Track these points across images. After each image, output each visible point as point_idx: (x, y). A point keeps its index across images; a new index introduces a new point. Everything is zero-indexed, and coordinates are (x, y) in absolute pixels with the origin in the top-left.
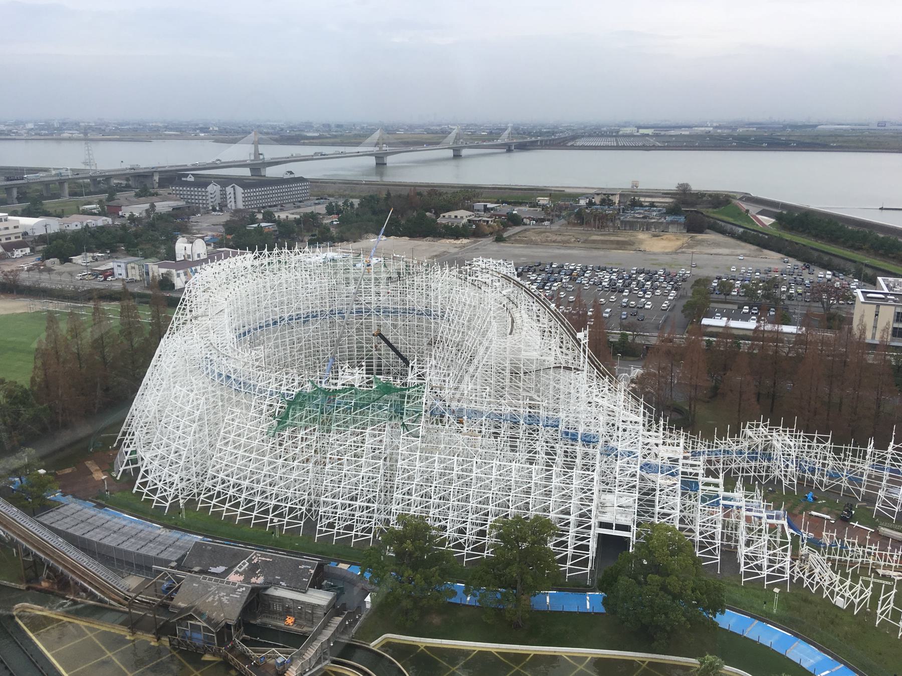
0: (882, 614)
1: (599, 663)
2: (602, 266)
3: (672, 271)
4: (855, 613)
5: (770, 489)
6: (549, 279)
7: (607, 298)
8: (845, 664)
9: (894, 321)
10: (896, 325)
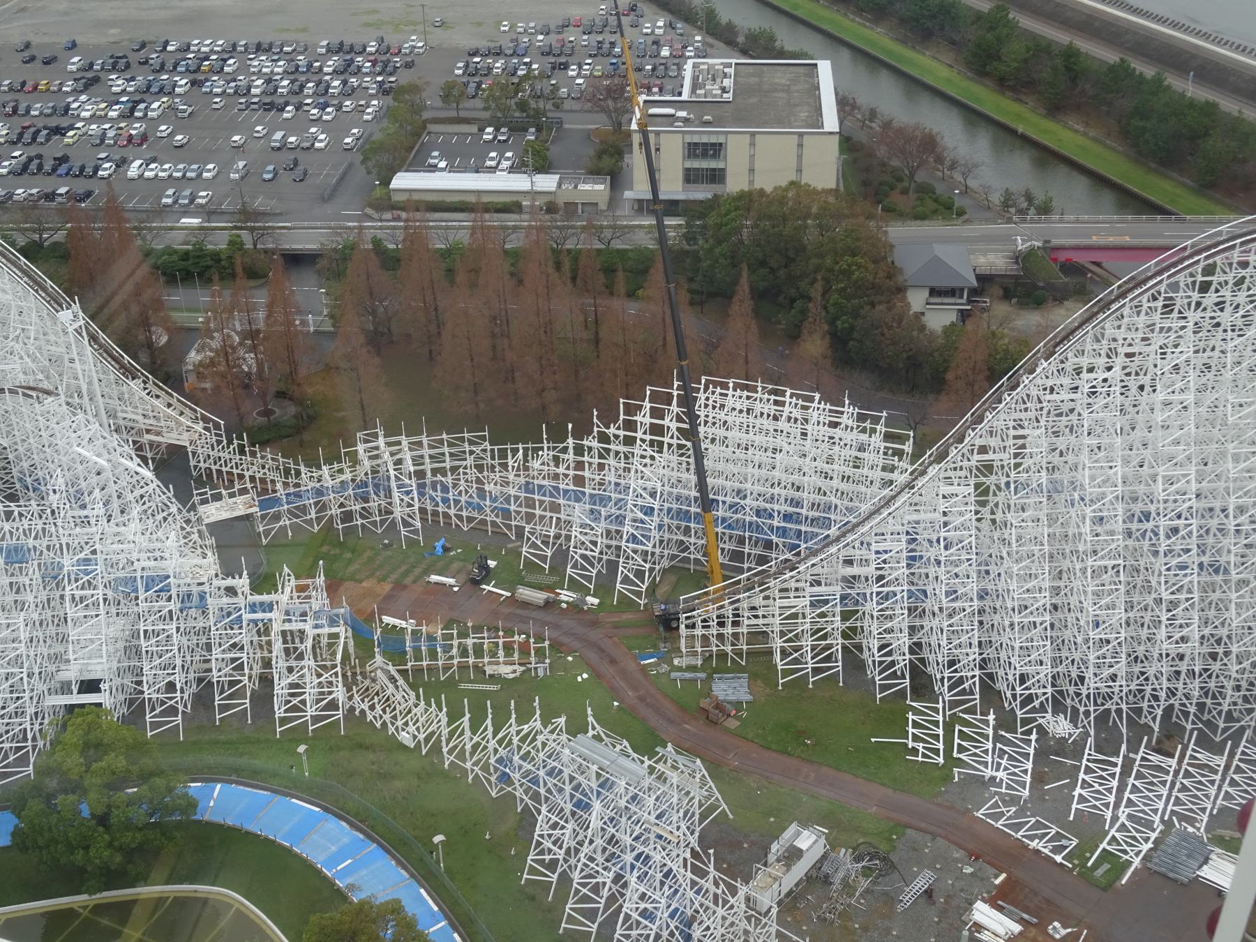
0: (450, 752)
1: (58, 919)
2: (266, 40)
3: (392, 39)
4: (424, 753)
5: (386, 541)
6: (149, 87)
7: (248, 130)
8: (380, 844)
9: (684, 157)
10: (688, 164)
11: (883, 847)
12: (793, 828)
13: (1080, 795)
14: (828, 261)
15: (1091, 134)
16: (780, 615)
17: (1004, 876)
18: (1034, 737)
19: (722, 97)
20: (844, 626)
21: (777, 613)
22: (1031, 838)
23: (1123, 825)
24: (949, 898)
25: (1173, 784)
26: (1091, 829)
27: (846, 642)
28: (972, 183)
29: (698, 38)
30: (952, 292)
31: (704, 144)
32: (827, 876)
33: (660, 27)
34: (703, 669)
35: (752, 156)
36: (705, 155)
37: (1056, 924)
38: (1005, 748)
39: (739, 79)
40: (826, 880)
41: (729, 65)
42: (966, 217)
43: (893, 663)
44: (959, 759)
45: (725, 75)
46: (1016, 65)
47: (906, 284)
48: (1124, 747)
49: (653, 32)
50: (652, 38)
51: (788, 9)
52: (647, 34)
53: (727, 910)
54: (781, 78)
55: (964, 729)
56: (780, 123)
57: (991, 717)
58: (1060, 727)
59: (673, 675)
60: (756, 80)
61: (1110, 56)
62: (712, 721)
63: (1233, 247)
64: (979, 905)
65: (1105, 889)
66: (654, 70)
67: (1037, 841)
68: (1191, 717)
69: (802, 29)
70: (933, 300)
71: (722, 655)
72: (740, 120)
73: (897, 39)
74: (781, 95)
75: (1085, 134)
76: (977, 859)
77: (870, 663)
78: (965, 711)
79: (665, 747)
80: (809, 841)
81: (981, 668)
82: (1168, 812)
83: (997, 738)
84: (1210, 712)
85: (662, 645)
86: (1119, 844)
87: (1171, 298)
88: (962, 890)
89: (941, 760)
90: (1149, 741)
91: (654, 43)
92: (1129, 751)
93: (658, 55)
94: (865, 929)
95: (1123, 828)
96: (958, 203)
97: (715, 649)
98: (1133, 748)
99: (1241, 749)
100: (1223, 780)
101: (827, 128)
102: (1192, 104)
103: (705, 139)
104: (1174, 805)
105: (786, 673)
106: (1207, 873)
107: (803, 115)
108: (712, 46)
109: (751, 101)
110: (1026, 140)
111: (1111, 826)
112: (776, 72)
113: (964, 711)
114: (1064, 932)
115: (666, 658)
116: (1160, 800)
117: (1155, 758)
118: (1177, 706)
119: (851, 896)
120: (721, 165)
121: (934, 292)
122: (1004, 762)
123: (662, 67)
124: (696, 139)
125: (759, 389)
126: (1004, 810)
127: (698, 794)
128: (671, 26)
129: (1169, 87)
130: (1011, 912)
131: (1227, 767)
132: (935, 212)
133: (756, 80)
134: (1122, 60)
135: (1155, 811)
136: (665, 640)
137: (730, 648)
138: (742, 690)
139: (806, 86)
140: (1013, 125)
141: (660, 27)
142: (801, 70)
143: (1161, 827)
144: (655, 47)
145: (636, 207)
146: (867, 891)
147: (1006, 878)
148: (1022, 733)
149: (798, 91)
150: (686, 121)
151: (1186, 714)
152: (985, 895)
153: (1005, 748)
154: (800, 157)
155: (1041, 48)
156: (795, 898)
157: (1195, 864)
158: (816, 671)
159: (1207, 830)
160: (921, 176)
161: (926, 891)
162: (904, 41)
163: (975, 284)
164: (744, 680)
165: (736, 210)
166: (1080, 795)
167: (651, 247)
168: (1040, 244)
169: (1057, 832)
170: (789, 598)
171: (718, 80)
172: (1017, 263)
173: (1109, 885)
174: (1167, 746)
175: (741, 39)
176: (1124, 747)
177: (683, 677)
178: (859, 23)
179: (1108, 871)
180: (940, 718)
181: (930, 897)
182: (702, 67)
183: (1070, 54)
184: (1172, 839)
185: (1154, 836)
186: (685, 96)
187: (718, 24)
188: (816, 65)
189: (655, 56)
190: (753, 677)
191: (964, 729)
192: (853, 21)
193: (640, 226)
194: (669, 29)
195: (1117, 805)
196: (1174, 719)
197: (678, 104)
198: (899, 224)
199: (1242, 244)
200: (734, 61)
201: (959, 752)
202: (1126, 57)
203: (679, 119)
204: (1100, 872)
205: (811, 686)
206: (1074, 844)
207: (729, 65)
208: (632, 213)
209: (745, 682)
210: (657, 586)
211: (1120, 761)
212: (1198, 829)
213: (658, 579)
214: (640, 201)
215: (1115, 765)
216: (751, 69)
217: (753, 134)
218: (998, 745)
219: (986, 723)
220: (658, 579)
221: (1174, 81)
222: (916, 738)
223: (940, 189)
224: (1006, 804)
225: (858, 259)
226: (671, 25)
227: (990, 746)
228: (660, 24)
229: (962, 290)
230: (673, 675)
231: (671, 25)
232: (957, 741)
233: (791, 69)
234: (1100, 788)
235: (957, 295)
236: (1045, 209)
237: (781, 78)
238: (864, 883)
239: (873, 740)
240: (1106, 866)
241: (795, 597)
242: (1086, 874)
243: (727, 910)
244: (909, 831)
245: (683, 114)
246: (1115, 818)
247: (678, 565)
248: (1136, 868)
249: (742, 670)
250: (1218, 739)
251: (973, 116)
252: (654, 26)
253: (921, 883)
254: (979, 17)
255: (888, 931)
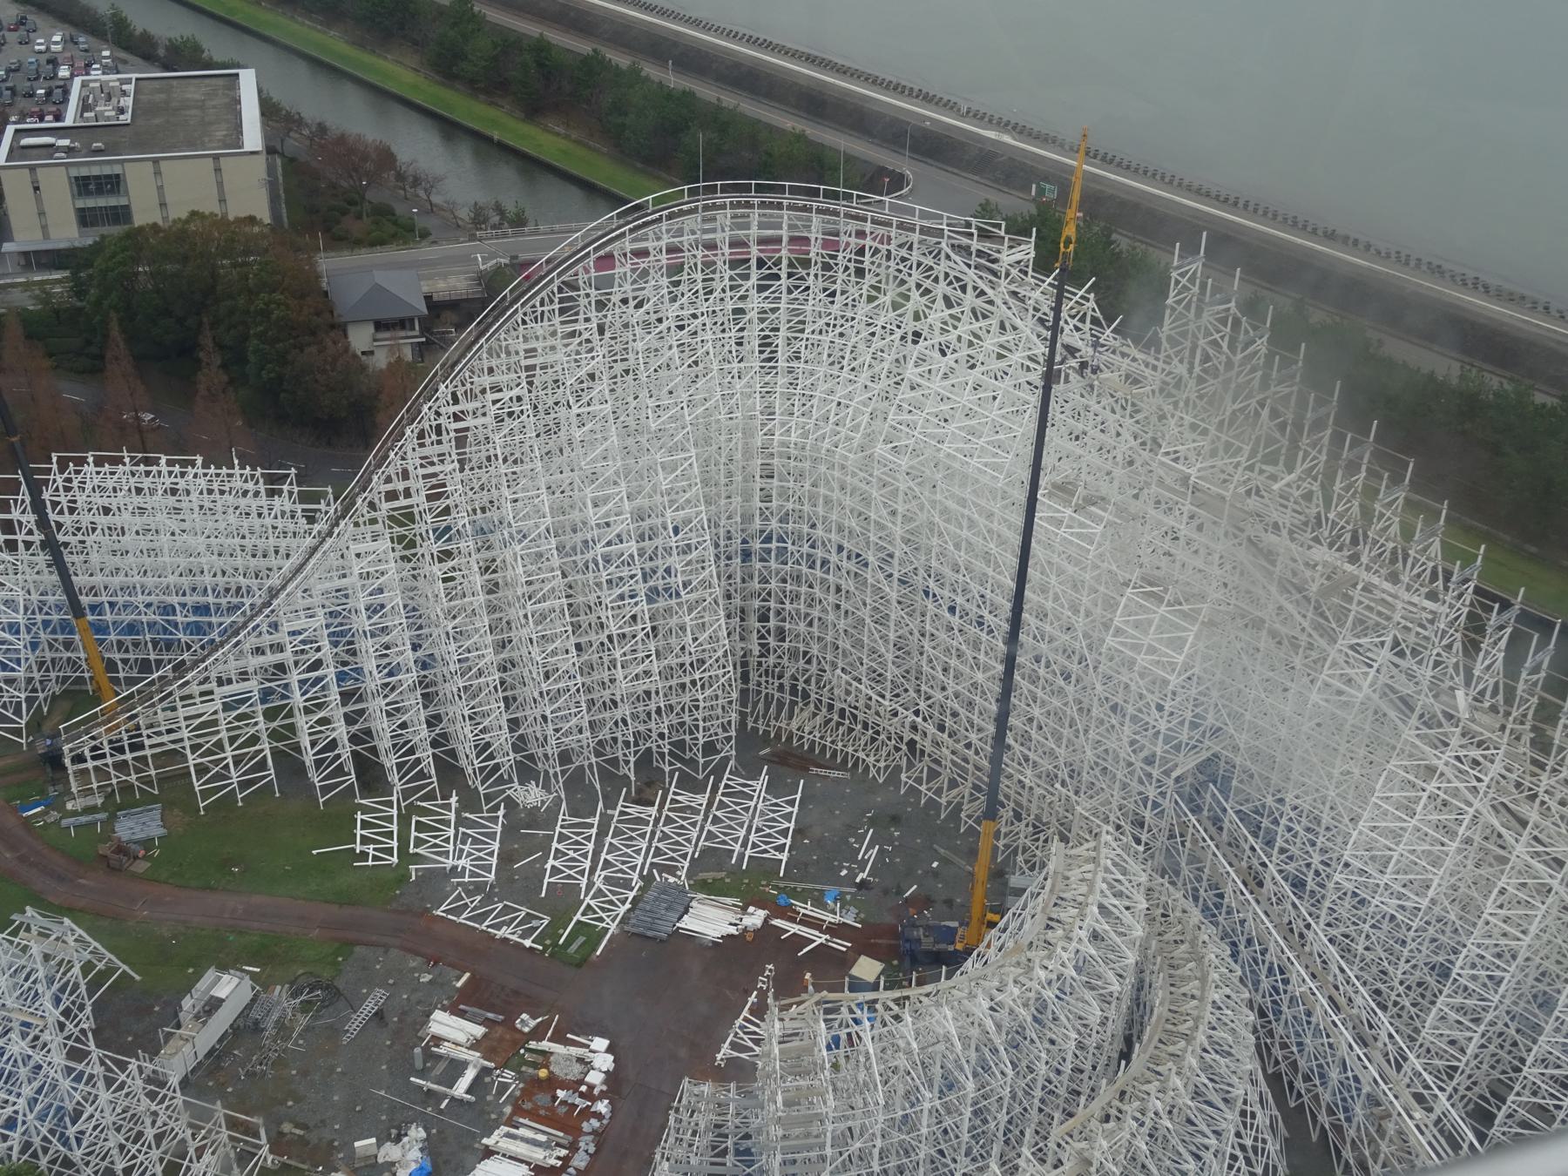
9: (73, 196)
10: (81, 204)
11: (326, 974)
12: (211, 974)
13: (553, 867)
14: (241, 301)
15: (573, 136)
16: (187, 727)
17: (467, 975)
18: (501, 813)
19: (118, 119)
20: (433, 734)
21: (183, 724)
22: (498, 927)
23: (600, 890)
24: (403, 1014)
25: (653, 833)
26: (564, 900)
27: (358, 748)
28: (435, 199)
29: (106, 53)
30: (403, 324)
31: (97, 177)
32: (256, 1023)
33: (56, 43)
34: (104, 808)
35: (160, 188)
36: (100, 191)
37: (524, 1016)
38: (468, 831)
39: (142, 97)
40: (257, 1028)
41: (128, 81)
42: (431, 238)
43: (497, 767)
44: (417, 854)
45: (124, 93)
46: (484, 63)
47: (343, 320)
48: (601, 805)
49: (48, 49)
50: (46, 56)
51: (223, 14)
52: (40, 52)
53: (114, 1092)
54: (194, 93)
55: (421, 819)
56: (193, 146)
57: (454, 800)
58: (531, 796)
59: (64, 822)
60: (163, 96)
61: (584, 47)
62: (113, 869)
63: (623, 234)
64: (438, 1015)
65: (579, 966)
66: (49, 94)
67: (505, 928)
68: (667, 757)
69: (246, 37)
70: (380, 335)
71: (126, 788)
72: (140, 144)
73: (354, 43)
74: (193, 112)
75: (567, 137)
76: (436, 963)
77: (471, 771)
78: (424, 798)
79: (24, 912)
80: (229, 987)
81: (598, 754)
82: (647, 866)
83: (461, 822)
84: (691, 750)
85: (51, 789)
86: (595, 912)
87: (571, 299)
88: (419, 1003)
89: (395, 860)
90: (628, 792)
91: (49, 62)
92: (606, 807)
93: (55, 76)
94: (304, 1073)
95: (600, 893)
96: (421, 223)
97: (114, 781)
98: (610, 803)
99: (724, 781)
100: (705, 820)
101: (248, 147)
102: (669, 95)
103: (95, 171)
104: (653, 857)
105: (206, 794)
106: (688, 923)
107: (220, 134)
108: (125, 62)
109: (157, 121)
110: (503, 147)
111: (586, 896)
112: (189, 85)
113: (422, 799)
114: (533, 1023)
115: (56, 804)
116: (639, 854)
117: (634, 810)
118: (655, 749)
119: (287, 1038)
120: (123, 201)
121: (380, 326)
122: (466, 848)
123: (60, 90)
124: (84, 172)
125: (127, 460)
126: (468, 901)
127: (79, 958)
128: (70, 41)
129: (647, 79)
130: (475, 1015)
131: (710, 804)
132: (394, 236)
133: (163, 96)
134: (595, 50)
135: (633, 868)
136: (54, 782)
137: (134, 777)
138: (154, 824)
139: (227, 100)
140: (488, 132)
141: (56, 43)
142: (220, 82)
143: (641, 883)
144: (50, 66)
145: (23, 262)
146: (307, 1029)
147: (469, 979)
148: (488, 811)
149: (214, 107)
150: (69, 151)
151: (662, 755)
152: (445, 1002)
153: (468, 831)
154: (220, 184)
155: (510, 44)
156: (218, 1057)
157: (673, 916)
158: (244, 785)
159: (688, 876)
160: (373, 196)
161: (376, 1014)
162: (360, 44)
163: (425, 311)
164: (156, 812)
165: (123, 251)
166: (553, 867)
167: (31, 308)
168: (507, 261)
169: (528, 914)
170: (195, 704)
171: (114, 100)
172: (480, 284)
173: (582, 962)
174: (648, 793)
175: (161, 52)
176: (601, 805)
177: (77, 823)
178: (309, 27)
179: (585, 942)
180: (395, 812)
181: (382, 1018)
182: (92, 85)
183: (541, 49)
184: (651, 894)
185: (631, 895)
186: (69, 121)
187: (131, 35)
188: (237, 75)
189: (51, 78)
190: (168, 806)
191: (421, 819)
192: (303, 24)
193: (13, 285)
194: (71, 45)
195: (593, 870)
196: (655, 763)
197: (62, 132)
198: (346, 253)
199: (631, 231)
200: (134, 76)
201: (416, 846)
202: (599, 47)
203: (59, 149)
204: (574, 947)
205: (240, 804)
206: (546, 922)
207: (128, 81)
208: (18, 269)
209: (157, 814)
210: (44, 718)
211: (596, 820)
212: (680, 877)
213: (45, 710)
214: (26, 254)
215: (592, 826)
216: (156, 84)
217: (156, 161)
218: (461, 830)
219: (448, 807)
220: (45, 710)
221: (651, 70)
222: (365, 840)
223: (400, 209)
224: (470, 894)
225: (277, 296)
226: (72, 39)
227: (451, 832)
228: (57, 38)
229: (412, 320)
230: (64, 822)
231: (72, 39)
232: (414, 834)
233: (207, 81)
234: (575, 855)
235: (408, 325)
236: (519, 222)
237: (194, 93)
238: (303, 1020)
239: (314, 852)
240: (582, 939)
241: (202, 702)
242: (558, 953)
243: (114, 1092)
244: (357, 949)
245: (66, 142)
246: (590, 885)
247: (72, 688)
248: (613, 935)
249: (154, 799)
250: (700, 777)
251: (450, 128)
252: (49, 42)
253: (369, 1007)
254: (441, 11)
255: (332, 1069)
